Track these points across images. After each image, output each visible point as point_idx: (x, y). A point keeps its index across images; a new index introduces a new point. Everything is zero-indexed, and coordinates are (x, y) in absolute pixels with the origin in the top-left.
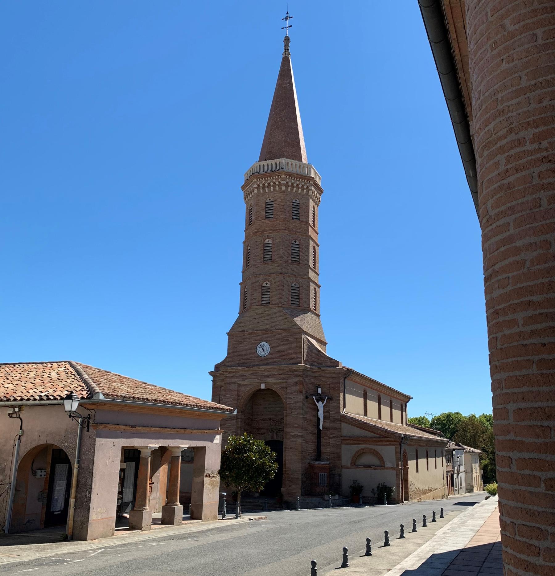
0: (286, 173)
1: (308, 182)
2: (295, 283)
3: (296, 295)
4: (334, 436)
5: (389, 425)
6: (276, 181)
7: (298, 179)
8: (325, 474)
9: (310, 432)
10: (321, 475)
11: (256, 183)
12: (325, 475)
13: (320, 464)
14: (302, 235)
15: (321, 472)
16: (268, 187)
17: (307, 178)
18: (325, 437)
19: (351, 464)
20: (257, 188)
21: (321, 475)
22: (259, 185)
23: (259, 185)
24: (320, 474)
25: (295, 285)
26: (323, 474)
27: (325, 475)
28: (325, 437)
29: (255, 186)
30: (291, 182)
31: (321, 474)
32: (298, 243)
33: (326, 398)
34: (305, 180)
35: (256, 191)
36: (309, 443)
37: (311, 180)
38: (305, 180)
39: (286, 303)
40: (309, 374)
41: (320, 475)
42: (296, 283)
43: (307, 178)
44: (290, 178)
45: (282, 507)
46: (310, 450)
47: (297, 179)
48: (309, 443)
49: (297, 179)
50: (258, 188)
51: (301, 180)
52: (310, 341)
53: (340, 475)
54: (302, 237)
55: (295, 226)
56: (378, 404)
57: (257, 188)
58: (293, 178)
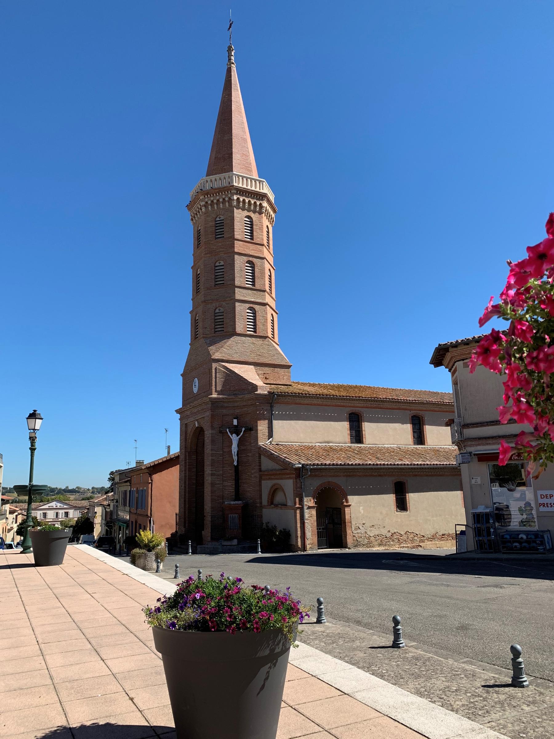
0: (203, 193)
1: (229, 192)
2: (219, 308)
3: (221, 320)
4: (255, 471)
5: (413, 453)
6: (208, 200)
7: (217, 194)
8: (236, 515)
9: (230, 468)
10: (232, 516)
11: (202, 201)
12: (236, 517)
13: (230, 504)
14: (225, 254)
15: (231, 514)
16: (211, 205)
17: (225, 189)
18: (248, 474)
19: (268, 503)
20: (205, 206)
21: (232, 516)
22: (207, 203)
23: (207, 203)
24: (229, 515)
25: (219, 310)
26: (234, 515)
27: (236, 517)
28: (248, 474)
29: (203, 203)
30: (210, 200)
31: (232, 515)
32: (222, 263)
33: (243, 429)
34: (225, 192)
35: (203, 209)
36: (229, 481)
37: (231, 189)
38: (225, 192)
39: (208, 332)
40: (226, 405)
41: (229, 517)
42: (220, 308)
43: (225, 189)
44: (209, 196)
45: (197, 552)
46: (231, 488)
47: (216, 194)
48: (229, 481)
49: (216, 194)
50: (206, 206)
51: (220, 194)
52: (228, 368)
53: (261, 517)
54: (226, 255)
55: (218, 246)
56: (351, 428)
57: (205, 206)
58: (212, 195)
